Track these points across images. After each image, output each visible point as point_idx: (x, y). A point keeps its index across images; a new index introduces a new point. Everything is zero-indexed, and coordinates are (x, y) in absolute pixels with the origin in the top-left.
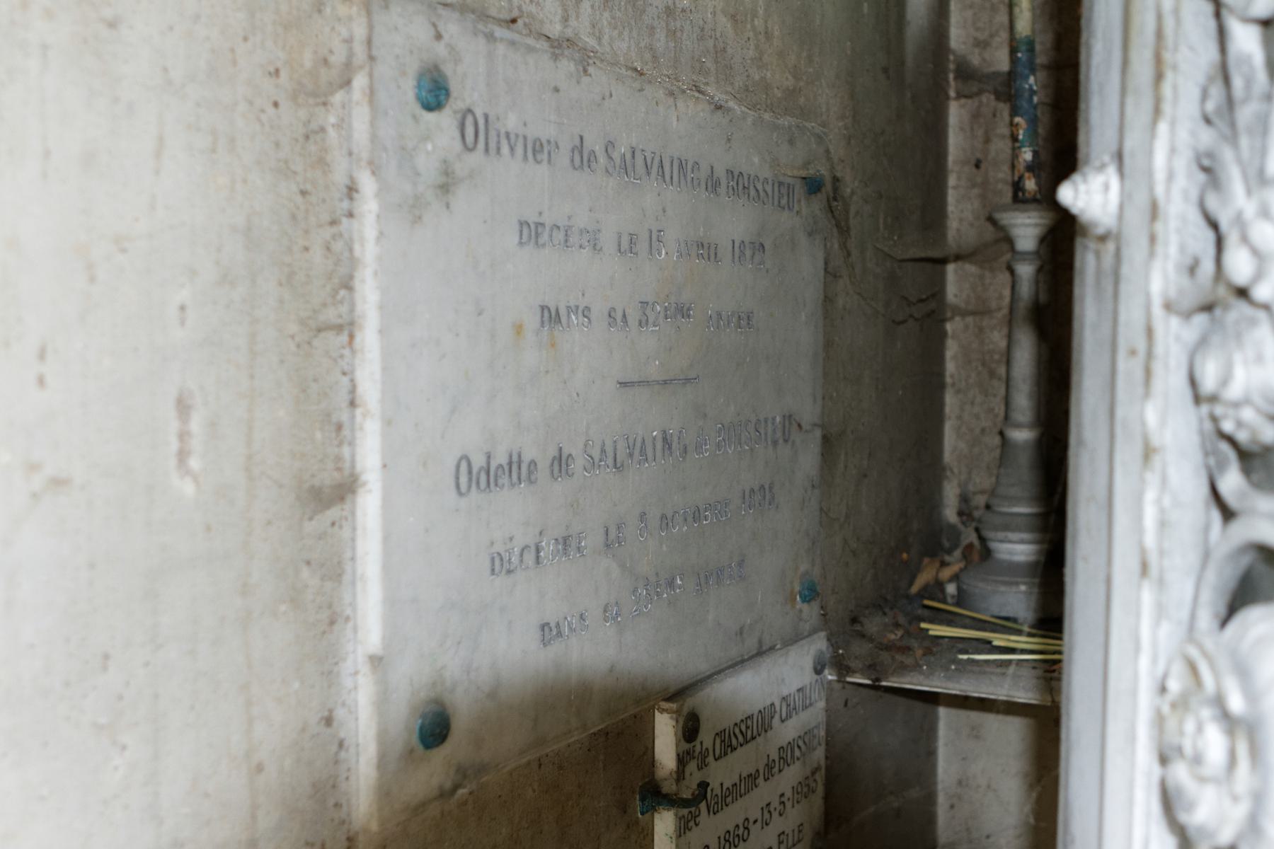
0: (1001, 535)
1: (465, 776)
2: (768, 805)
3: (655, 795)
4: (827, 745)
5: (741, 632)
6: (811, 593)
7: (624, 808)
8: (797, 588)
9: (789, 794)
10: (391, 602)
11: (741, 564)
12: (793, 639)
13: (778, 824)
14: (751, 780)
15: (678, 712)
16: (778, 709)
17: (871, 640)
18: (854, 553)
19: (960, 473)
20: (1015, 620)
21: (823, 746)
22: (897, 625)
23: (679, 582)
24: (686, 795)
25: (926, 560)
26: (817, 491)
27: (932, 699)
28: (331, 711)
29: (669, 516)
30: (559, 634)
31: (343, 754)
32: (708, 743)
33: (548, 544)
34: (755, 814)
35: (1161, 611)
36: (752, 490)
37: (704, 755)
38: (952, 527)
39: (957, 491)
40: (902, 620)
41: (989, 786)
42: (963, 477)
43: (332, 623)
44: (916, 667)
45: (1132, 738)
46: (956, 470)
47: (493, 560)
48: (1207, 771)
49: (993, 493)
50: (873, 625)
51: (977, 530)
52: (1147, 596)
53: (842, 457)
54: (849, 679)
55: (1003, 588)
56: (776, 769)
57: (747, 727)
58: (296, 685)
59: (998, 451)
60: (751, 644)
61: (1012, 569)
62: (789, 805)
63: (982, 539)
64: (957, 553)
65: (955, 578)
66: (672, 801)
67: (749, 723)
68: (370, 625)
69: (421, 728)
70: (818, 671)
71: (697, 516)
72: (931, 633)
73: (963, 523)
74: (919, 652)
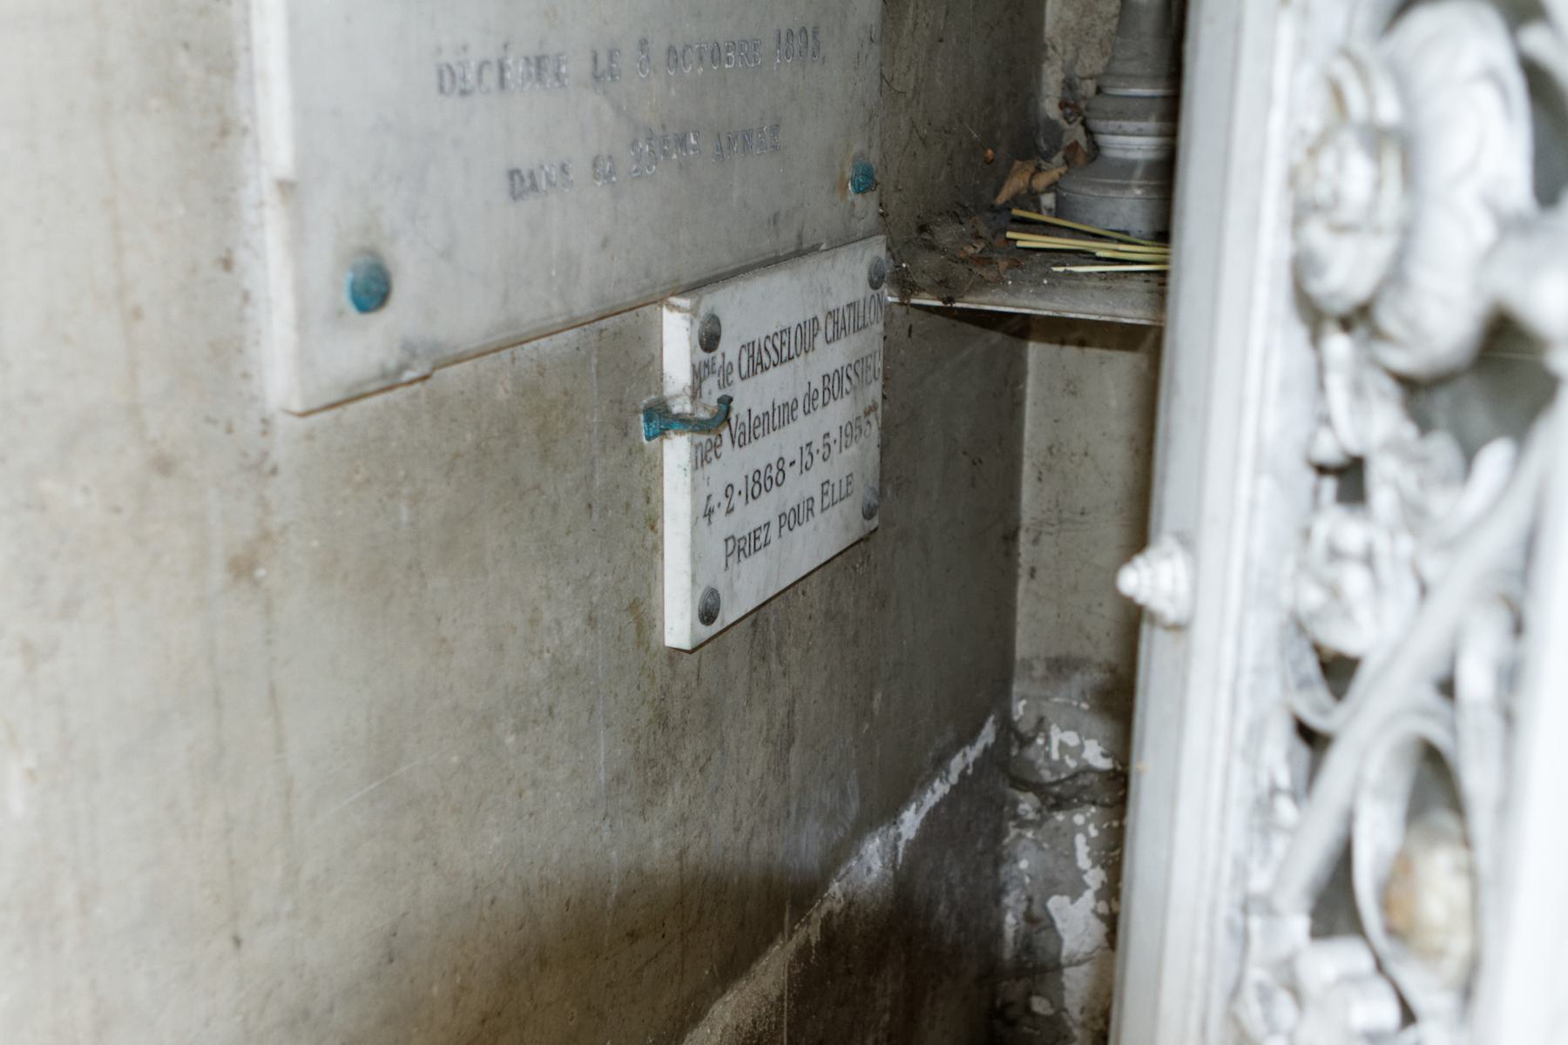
0: (1113, 124)
1: (414, 355)
2: (809, 445)
3: (662, 419)
4: (885, 378)
5: (775, 219)
6: (866, 181)
7: (625, 431)
8: (849, 174)
9: (835, 434)
10: (303, 110)
11: (775, 128)
12: (844, 240)
13: (820, 471)
14: (787, 412)
15: (693, 311)
16: (822, 325)
17: (943, 252)
18: (924, 140)
19: (1065, 52)
20: (1126, 233)
21: (880, 382)
22: (978, 237)
23: (693, 141)
24: (703, 415)
25: (1018, 163)
26: (876, 48)
27: (1022, 328)
28: (229, 251)
29: (679, 49)
30: (534, 187)
31: (249, 311)
32: (732, 356)
33: (516, 63)
34: (791, 453)
35: (1302, 49)
36: (790, 33)
37: (726, 371)
38: (1052, 124)
39: (1061, 76)
40: (983, 230)
41: (1086, 454)
42: (1069, 57)
43: (224, 132)
44: (999, 282)
45: (1255, 221)
46: (1060, 49)
47: (441, 75)
48: (1346, 215)
49: (1108, 72)
50: (946, 234)
51: (1084, 123)
52: (1287, 30)
53: (911, 10)
54: (914, 301)
55: (1112, 194)
56: (819, 402)
57: (783, 344)
58: (180, 210)
59: (1115, 21)
60: (787, 239)
61: (1127, 168)
62: (835, 448)
63: (1089, 133)
64: (1058, 158)
65: (1053, 187)
66: (686, 423)
67: (785, 338)
68: (276, 144)
69: (353, 285)
70: (875, 284)
71: (717, 55)
72: (1019, 244)
73: (1066, 118)
74: (1003, 264)
